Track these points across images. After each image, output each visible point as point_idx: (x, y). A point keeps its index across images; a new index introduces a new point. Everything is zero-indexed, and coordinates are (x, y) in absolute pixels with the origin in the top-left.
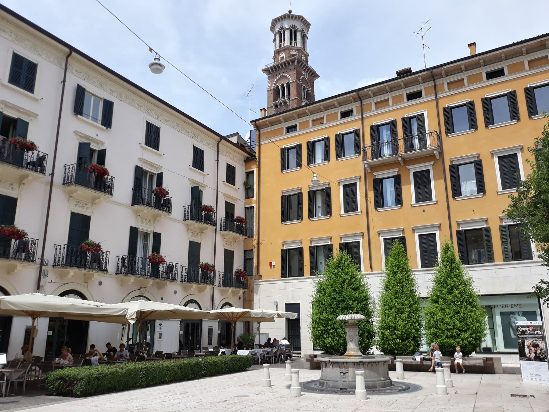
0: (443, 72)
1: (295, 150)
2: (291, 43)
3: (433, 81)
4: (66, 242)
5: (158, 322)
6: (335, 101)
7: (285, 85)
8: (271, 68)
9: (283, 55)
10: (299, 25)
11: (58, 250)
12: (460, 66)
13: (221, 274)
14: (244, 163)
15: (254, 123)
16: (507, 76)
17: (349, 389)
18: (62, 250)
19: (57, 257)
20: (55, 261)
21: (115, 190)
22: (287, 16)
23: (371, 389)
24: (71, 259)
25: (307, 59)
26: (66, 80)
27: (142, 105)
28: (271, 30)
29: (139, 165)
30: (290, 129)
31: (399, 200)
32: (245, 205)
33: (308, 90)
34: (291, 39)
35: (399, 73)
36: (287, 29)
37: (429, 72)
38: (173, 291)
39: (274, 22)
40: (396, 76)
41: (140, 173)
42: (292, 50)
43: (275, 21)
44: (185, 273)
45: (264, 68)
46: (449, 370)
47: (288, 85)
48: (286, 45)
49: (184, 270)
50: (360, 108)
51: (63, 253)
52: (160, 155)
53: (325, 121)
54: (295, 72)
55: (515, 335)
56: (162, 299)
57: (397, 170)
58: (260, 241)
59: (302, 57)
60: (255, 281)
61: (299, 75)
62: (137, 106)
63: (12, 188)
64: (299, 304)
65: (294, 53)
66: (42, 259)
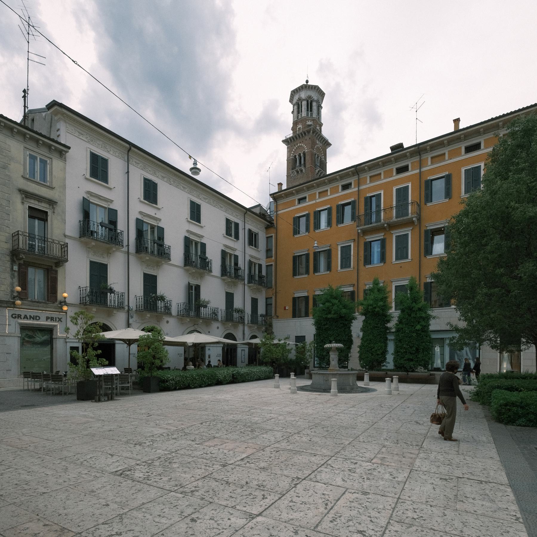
0: (428, 147)
1: (304, 218)
2: (308, 114)
3: (418, 156)
4: (142, 295)
5: (207, 348)
6: (337, 175)
7: (302, 154)
8: (290, 138)
9: (300, 126)
10: (315, 96)
11: (138, 300)
12: (443, 141)
13: (249, 315)
14: (265, 230)
15: (272, 196)
16: (483, 149)
17: (327, 390)
18: (141, 299)
19: (138, 304)
20: (137, 307)
21: (172, 257)
22: (304, 87)
23: (342, 389)
24: (147, 306)
25: (321, 129)
26: (130, 171)
27: (186, 187)
28: (290, 101)
29: (187, 236)
30: (300, 200)
31: (383, 258)
32: (266, 263)
33: (321, 159)
34: (308, 110)
35: (392, 148)
36: (304, 100)
37: (417, 148)
38: (216, 327)
39: (293, 93)
40: (390, 152)
41: (188, 242)
42: (308, 120)
43: (294, 93)
44: (224, 314)
45: (284, 139)
46: (397, 380)
47: (304, 154)
48: (303, 115)
49: (223, 312)
50: (357, 181)
51: (141, 302)
52: (202, 227)
53: (329, 194)
54: (310, 142)
55: (458, 359)
56: (209, 332)
57: (383, 234)
58: (277, 291)
59: (316, 127)
60: (273, 320)
61: (314, 144)
62: (182, 188)
63: (103, 257)
64: (305, 336)
65: (309, 123)
66: (128, 306)
